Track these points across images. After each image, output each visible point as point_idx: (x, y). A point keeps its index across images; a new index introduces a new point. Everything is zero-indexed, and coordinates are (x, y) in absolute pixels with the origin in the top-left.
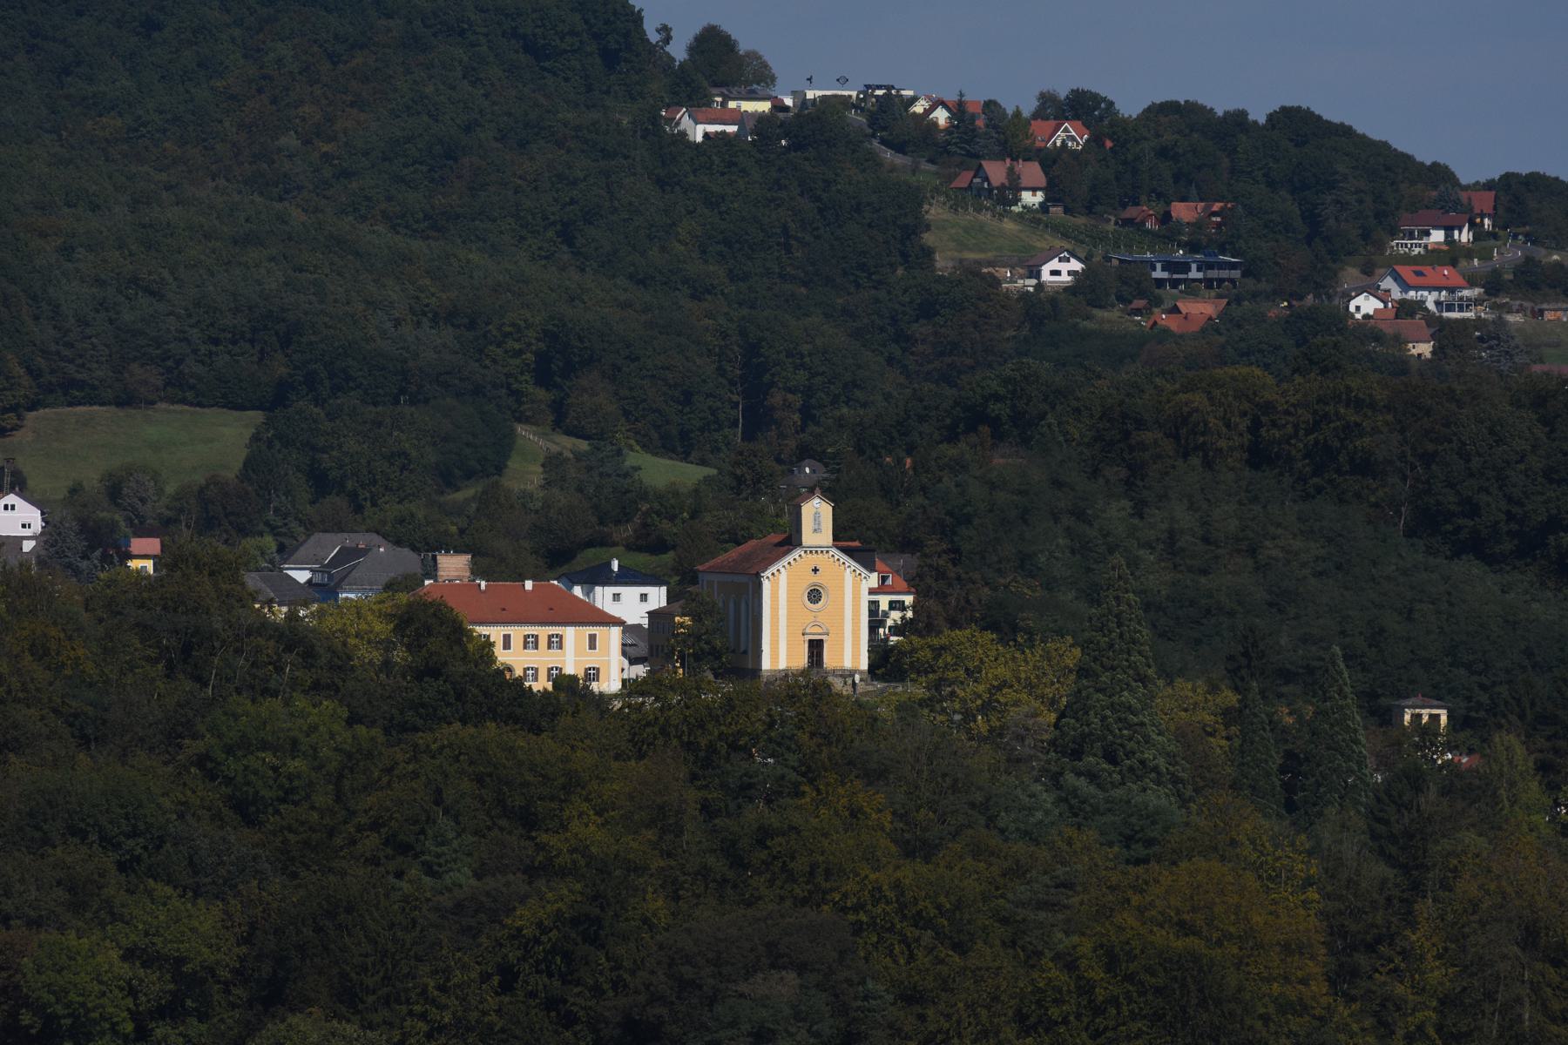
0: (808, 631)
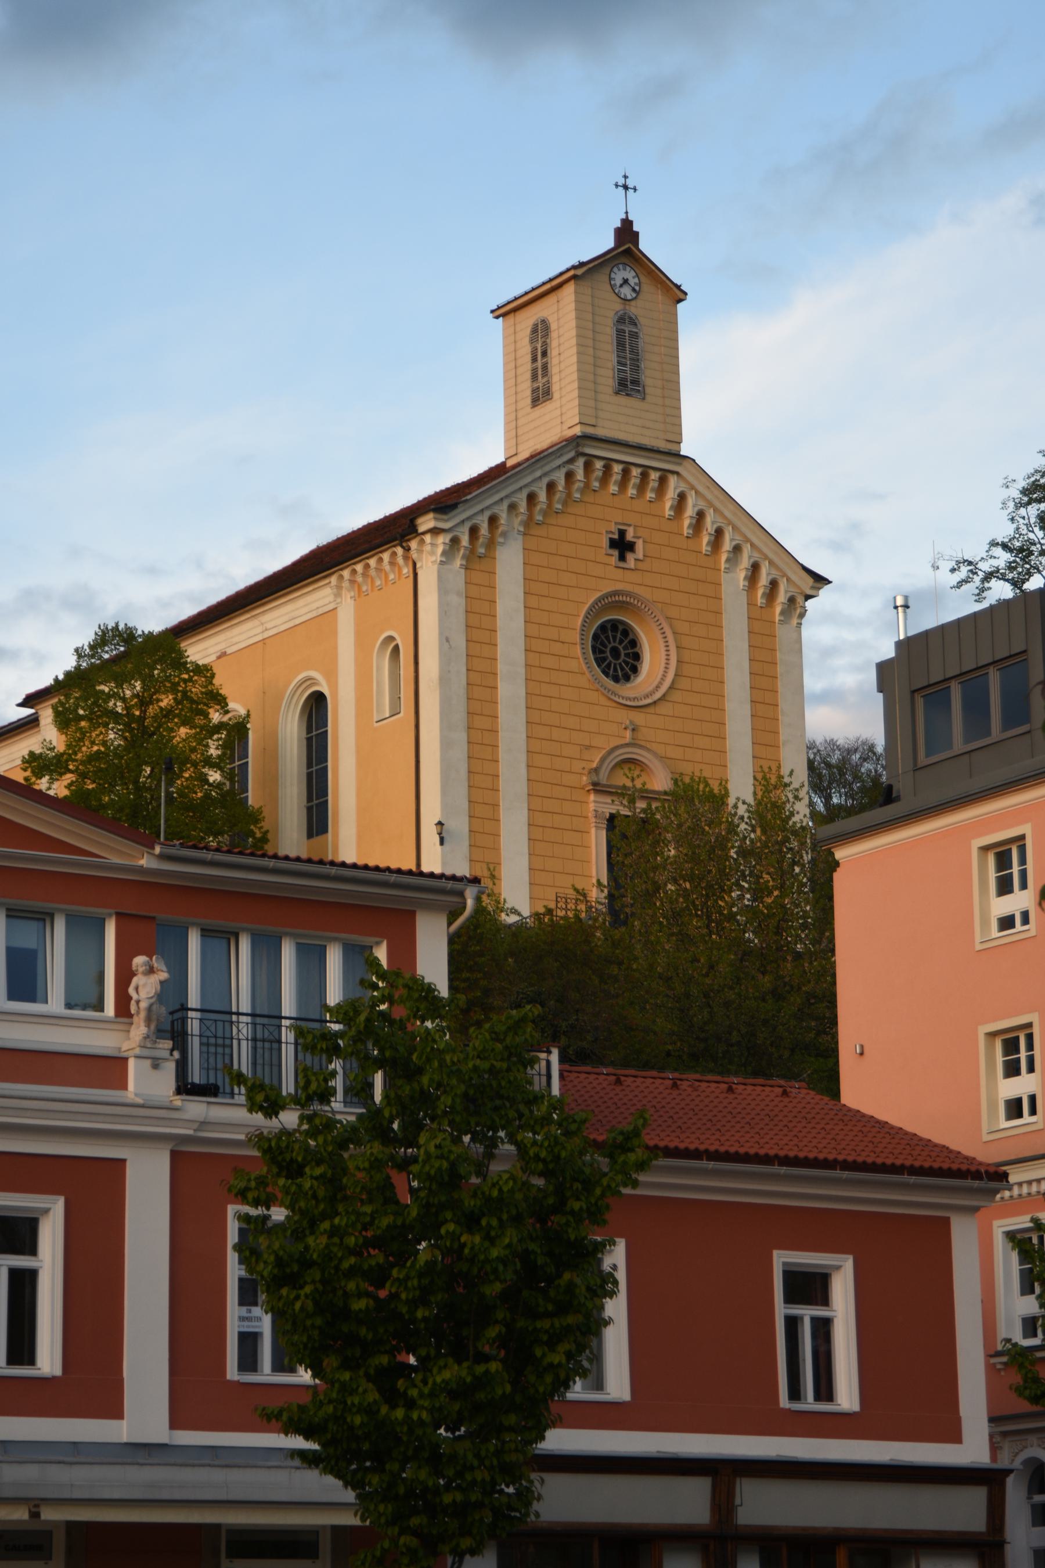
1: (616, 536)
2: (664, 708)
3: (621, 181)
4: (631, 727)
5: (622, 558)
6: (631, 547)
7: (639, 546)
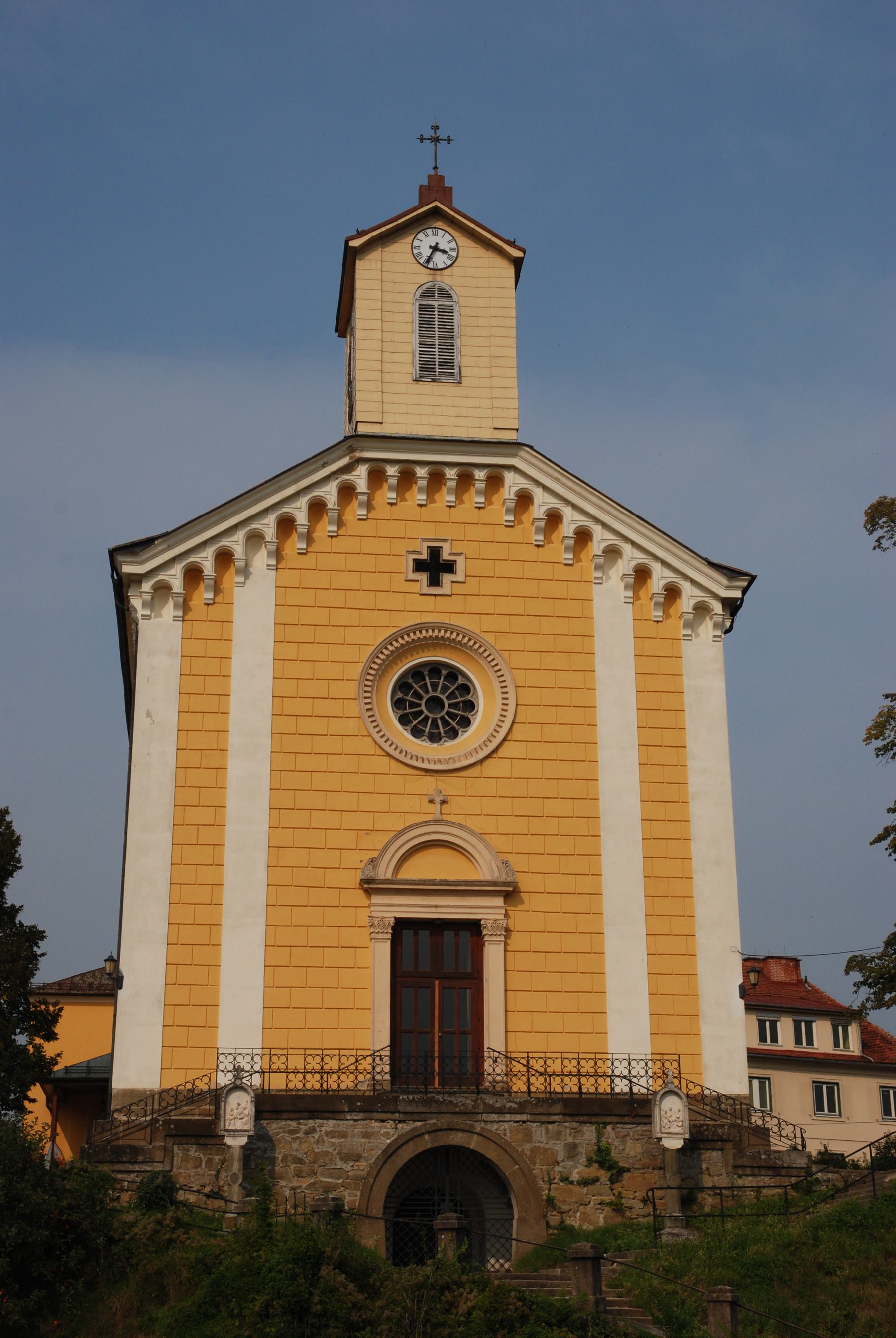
0: (385, 871)
1: (424, 556)
2: (493, 767)
3: (429, 133)
4: (438, 799)
5: (434, 581)
6: (450, 567)
7: (460, 567)
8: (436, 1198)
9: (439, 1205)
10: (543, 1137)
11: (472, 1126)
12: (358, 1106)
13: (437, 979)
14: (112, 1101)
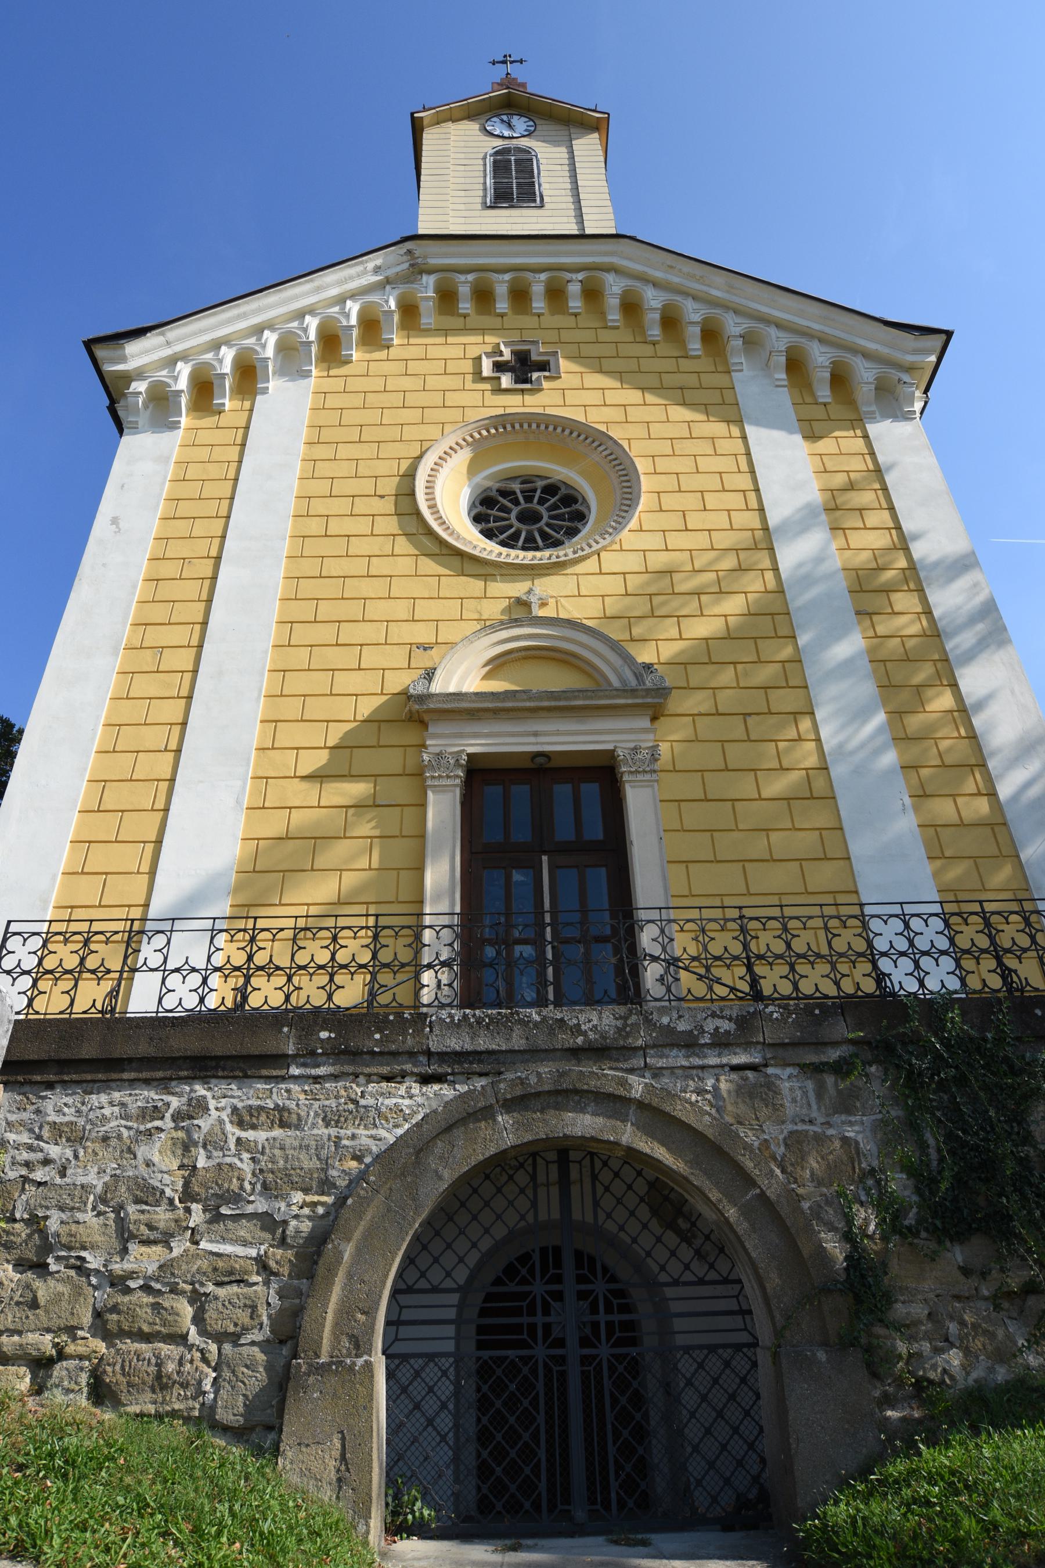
8: (538, 1288)
9: (546, 1312)
10: (814, 1106)
11: (623, 1083)
12: (322, 1041)
13: (545, 852)
14: (525, 1140)
